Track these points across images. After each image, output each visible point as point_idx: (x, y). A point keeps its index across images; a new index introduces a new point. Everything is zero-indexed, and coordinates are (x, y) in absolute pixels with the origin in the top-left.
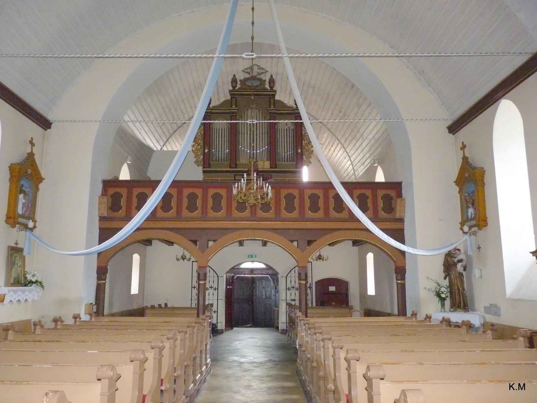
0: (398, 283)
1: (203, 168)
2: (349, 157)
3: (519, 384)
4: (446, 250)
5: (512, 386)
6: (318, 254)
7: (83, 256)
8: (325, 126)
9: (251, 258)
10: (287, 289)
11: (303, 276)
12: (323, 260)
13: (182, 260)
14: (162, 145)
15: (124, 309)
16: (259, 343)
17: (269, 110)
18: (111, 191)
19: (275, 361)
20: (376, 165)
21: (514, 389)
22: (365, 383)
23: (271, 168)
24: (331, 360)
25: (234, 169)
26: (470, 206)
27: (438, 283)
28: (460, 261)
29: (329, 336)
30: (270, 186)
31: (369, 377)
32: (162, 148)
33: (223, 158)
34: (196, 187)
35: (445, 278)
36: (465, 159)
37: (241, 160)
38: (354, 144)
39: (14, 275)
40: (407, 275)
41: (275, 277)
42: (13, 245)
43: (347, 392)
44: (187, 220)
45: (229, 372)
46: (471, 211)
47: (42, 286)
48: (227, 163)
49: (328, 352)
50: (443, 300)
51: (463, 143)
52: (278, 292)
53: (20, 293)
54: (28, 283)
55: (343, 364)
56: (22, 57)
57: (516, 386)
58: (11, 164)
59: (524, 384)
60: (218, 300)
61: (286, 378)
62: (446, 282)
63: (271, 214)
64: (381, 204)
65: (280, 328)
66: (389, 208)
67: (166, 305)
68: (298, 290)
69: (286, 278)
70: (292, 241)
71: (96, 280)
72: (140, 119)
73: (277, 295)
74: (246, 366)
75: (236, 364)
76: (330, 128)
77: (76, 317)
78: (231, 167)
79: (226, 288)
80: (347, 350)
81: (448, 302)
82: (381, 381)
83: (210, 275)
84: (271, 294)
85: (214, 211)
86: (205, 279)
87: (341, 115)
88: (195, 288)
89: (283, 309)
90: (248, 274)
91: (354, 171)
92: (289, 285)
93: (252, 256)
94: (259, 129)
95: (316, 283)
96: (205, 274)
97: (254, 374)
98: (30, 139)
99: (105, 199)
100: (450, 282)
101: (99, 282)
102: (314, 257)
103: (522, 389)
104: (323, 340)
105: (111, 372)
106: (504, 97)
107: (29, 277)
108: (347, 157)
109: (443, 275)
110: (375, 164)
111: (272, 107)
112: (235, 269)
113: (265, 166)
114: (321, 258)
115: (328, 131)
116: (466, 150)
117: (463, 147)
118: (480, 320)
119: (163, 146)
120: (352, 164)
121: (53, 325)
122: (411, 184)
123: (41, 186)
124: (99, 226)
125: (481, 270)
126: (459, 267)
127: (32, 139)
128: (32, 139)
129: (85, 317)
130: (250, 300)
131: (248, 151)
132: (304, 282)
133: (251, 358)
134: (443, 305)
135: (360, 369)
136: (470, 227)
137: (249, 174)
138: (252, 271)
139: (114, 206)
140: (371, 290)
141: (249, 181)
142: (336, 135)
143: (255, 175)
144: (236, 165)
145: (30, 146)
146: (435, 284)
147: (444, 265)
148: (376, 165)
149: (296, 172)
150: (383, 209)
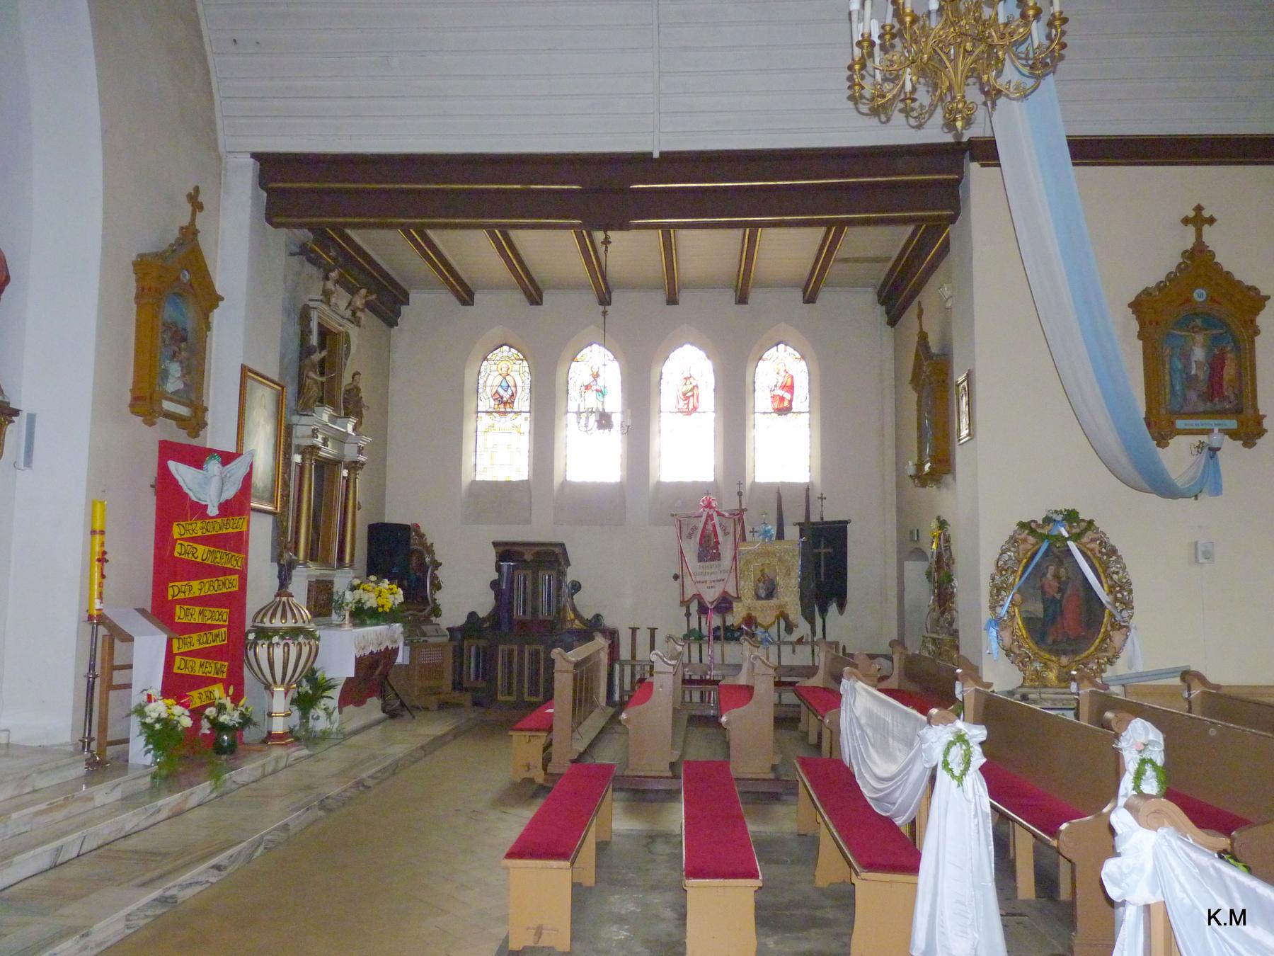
21: (1219, 924)
57: (1224, 917)
59: (1244, 911)
103: (1238, 923)
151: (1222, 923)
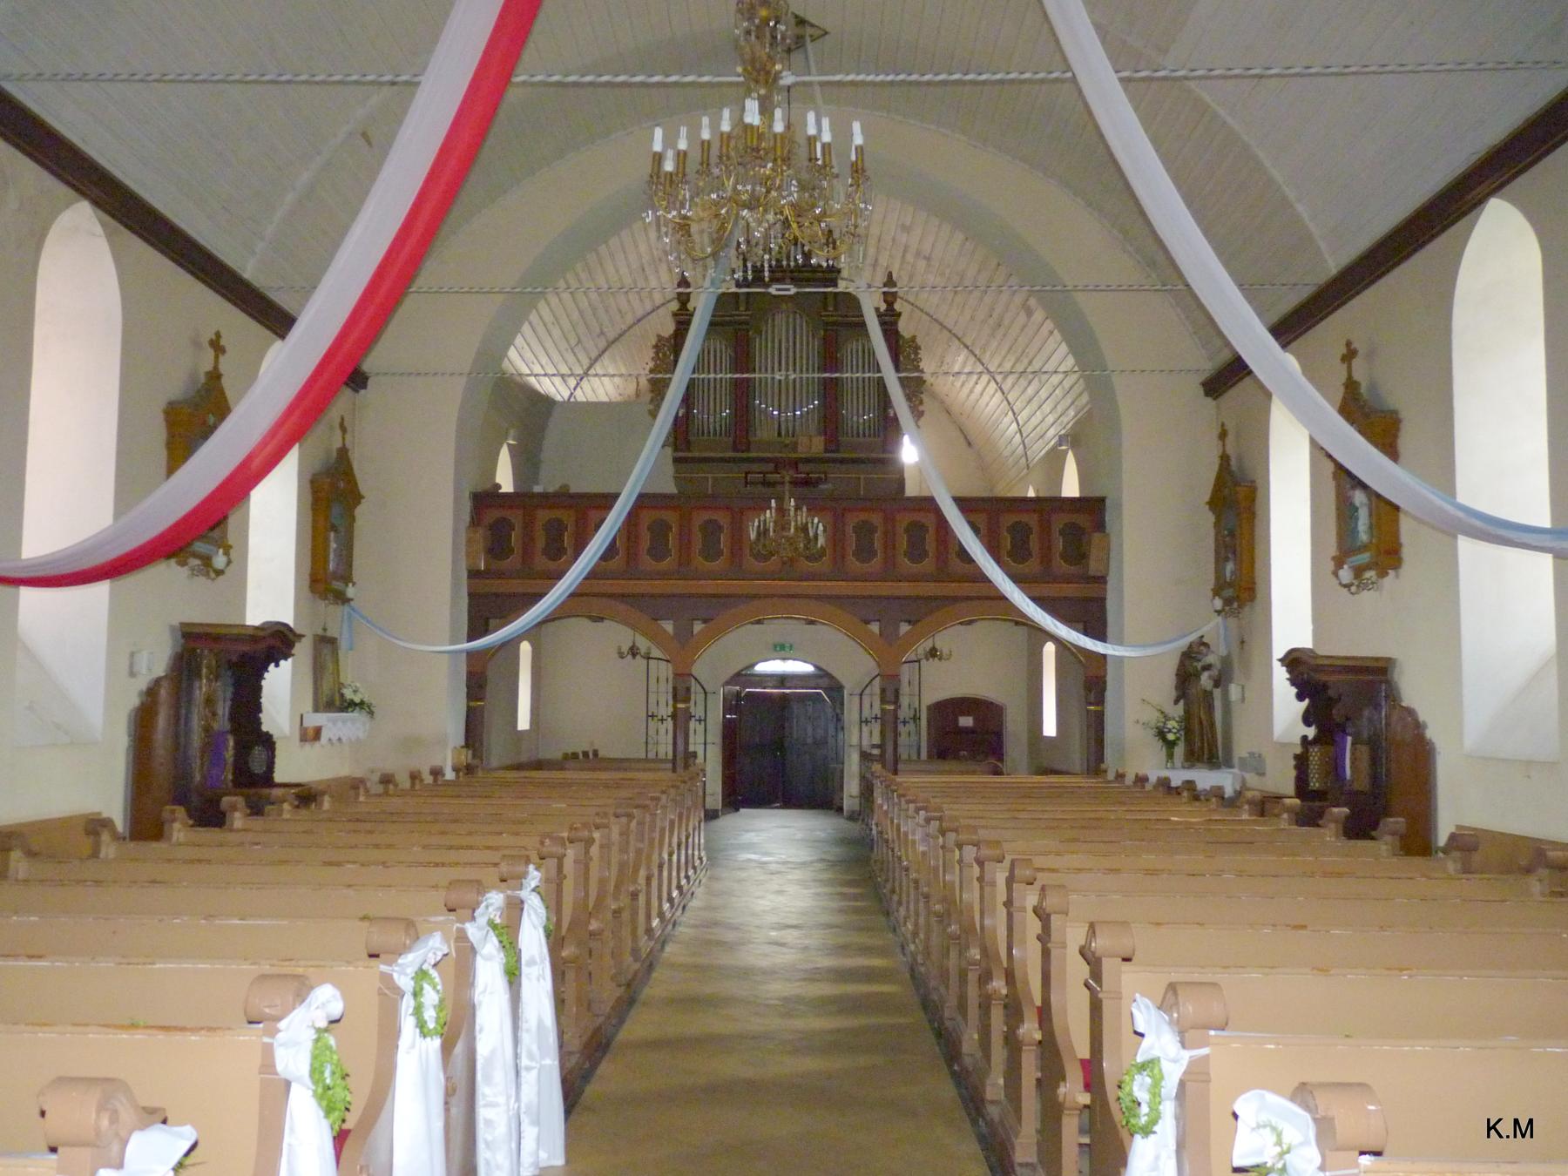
0: (1091, 710)
1: (676, 450)
2: (1014, 414)
3: (1516, 1122)
4: (1183, 644)
5: (1494, 1127)
6: (928, 645)
7: (446, 655)
8: (959, 339)
9: (781, 650)
10: (861, 722)
11: (890, 693)
12: (940, 659)
13: (630, 657)
14: (572, 386)
15: (509, 762)
16: (799, 836)
17: (825, 316)
18: (492, 515)
19: (829, 861)
20: (1064, 448)
21: (1501, 1136)
22: (1084, 970)
23: (826, 451)
24: (1002, 912)
25: (744, 455)
26: (1230, 555)
27: (1162, 713)
28: (1208, 667)
29: (998, 852)
30: (821, 525)
31: (1093, 953)
32: (572, 394)
33: (718, 428)
34: (666, 508)
35: (1176, 702)
36: (1225, 459)
37: (758, 432)
38: (1022, 388)
39: (327, 686)
40: (1109, 694)
41: (835, 694)
42: (320, 632)
43: (1084, 1052)
44: (651, 576)
45: (743, 875)
46: (1230, 567)
47: (371, 713)
48: (726, 439)
49: (994, 897)
50: (1170, 745)
51: (1348, 344)
52: (843, 728)
53: (340, 724)
54: (348, 706)
55: (1077, 970)
56: (142, 81)
57: (1506, 1127)
58: (314, 475)
59: (1531, 1121)
60: (705, 744)
61: (849, 884)
62: (1179, 710)
63: (824, 565)
64: (1059, 544)
65: (845, 808)
66: (1077, 552)
67: (596, 753)
68: (879, 721)
69: (861, 699)
70: (867, 622)
71: (465, 700)
72: (551, 370)
73: (840, 736)
74: (773, 867)
75: (753, 864)
76: (969, 344)
77: (437, 773)
78: (735, 450)
79: (724, 716)
80: (1043, 889)
81: (1179, 751)
82: (1126, 966)
83: (697, 695)
84: (826, 731)
85: (706, 559)
86: (687, 700)
87: (991, 321)
88: (660, 717)
89: (852, 764)
90: (772, 688)
91: (1025, 448)
92: (866, 713)
93: (782, 647)
94: (802, 344)
95: (929, 708)
96: (688, 690)
97: (790, 877)
98: (214, 337)
99: (480, 534)
100: (1187, 711)
101: (472, 704)
102: (921, 651)
103: (1523, 1136)
104: (960, 846)
105: (98, 1112)
106: (1503, 191)
107: (348, 694)
108: (1010, 413)
109: (1174, 694)
110: (1061, 445)
111: (831, 309)
112: (745, 675)
113: (813, 447)
114: (937, 656)
115: (966, 350)
116: (1356, 362)
117: (1349, 355)
118: (1233, 784)
119: (575, 389)
120: (1020, 430)
121: (380, 789)
122: (1119, 506)
123: (359, 511)
124: (469, 589)
125: (1243, 688)
126: (1205, 680)
127: (218, 335)
128: (218, 335)
129: (450, 775)
130: (778, 745)
131: (775, 413)
132: (892, 707)
133: (783, 857)
134: (1170, 756)
135: (1072, 935)
136: (1358, 572)
137: (780, 500)
138: (782, 680)
139: (497, 546)
140: (1050, 728)
141: (781, 511)
142: (984, 361)
143: (793, 503)
144: (749, 443)
145: (211, 353)
146: (1158, 714)
147: (1177, 675)
148: (1064, 448)
149: (884, 459)
150: (1064, 557)
151: (1504, 1135)
